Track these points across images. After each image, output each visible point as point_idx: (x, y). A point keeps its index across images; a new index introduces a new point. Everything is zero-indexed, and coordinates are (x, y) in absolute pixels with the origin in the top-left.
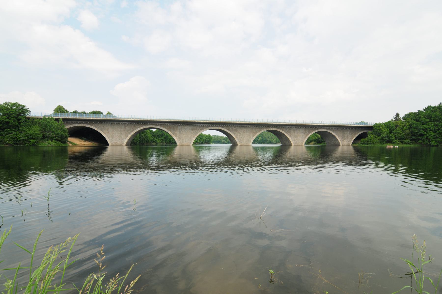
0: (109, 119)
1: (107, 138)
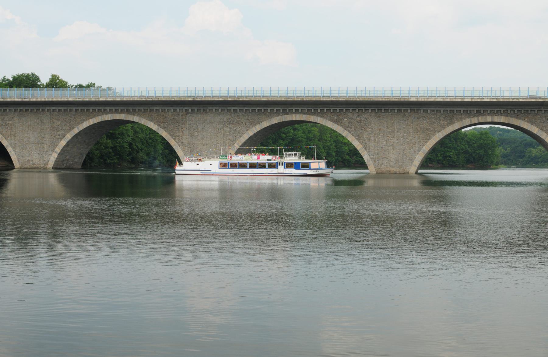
0: (9, 100)
1: (9, 150)
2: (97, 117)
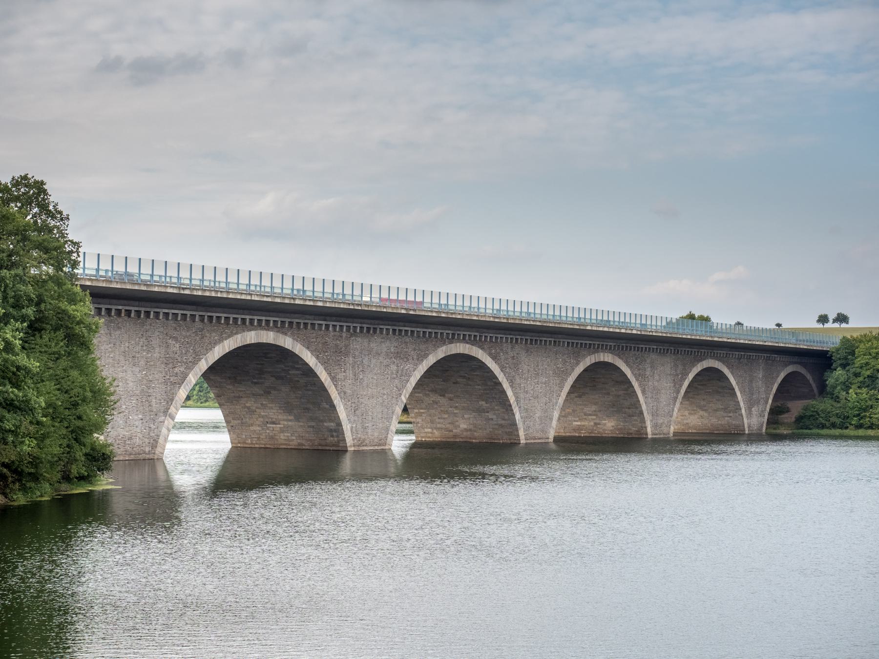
2: (235, 336)
